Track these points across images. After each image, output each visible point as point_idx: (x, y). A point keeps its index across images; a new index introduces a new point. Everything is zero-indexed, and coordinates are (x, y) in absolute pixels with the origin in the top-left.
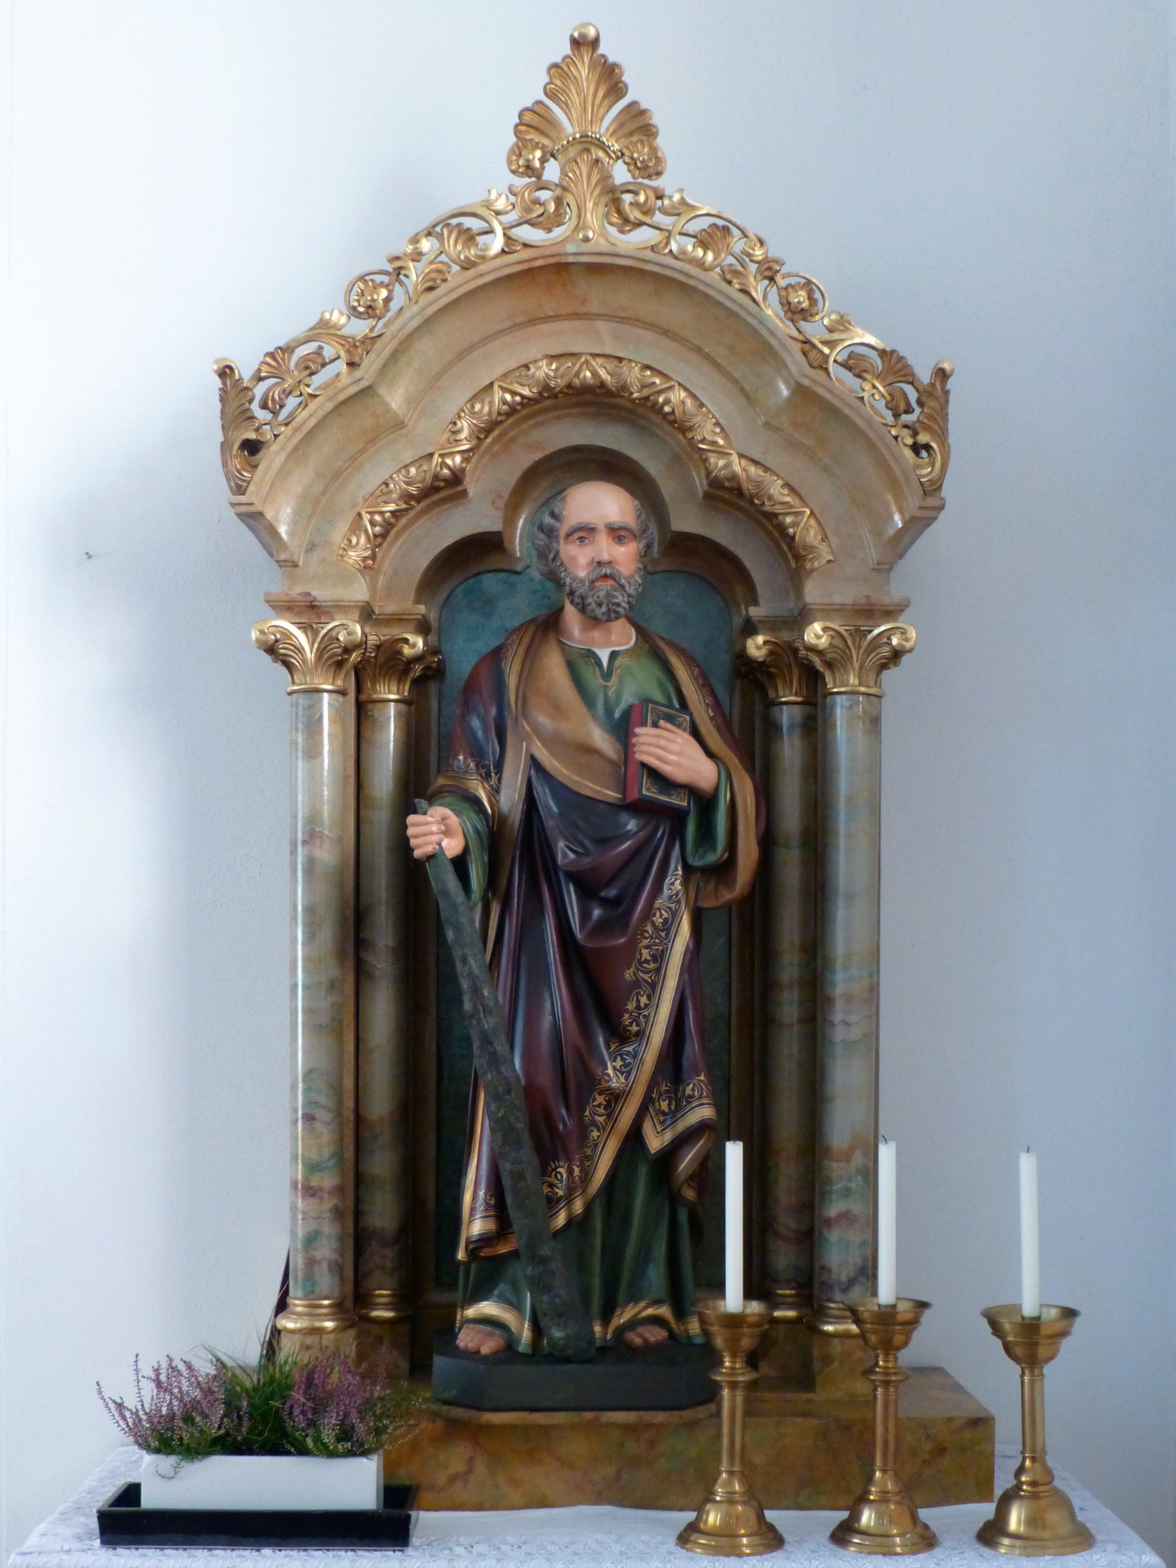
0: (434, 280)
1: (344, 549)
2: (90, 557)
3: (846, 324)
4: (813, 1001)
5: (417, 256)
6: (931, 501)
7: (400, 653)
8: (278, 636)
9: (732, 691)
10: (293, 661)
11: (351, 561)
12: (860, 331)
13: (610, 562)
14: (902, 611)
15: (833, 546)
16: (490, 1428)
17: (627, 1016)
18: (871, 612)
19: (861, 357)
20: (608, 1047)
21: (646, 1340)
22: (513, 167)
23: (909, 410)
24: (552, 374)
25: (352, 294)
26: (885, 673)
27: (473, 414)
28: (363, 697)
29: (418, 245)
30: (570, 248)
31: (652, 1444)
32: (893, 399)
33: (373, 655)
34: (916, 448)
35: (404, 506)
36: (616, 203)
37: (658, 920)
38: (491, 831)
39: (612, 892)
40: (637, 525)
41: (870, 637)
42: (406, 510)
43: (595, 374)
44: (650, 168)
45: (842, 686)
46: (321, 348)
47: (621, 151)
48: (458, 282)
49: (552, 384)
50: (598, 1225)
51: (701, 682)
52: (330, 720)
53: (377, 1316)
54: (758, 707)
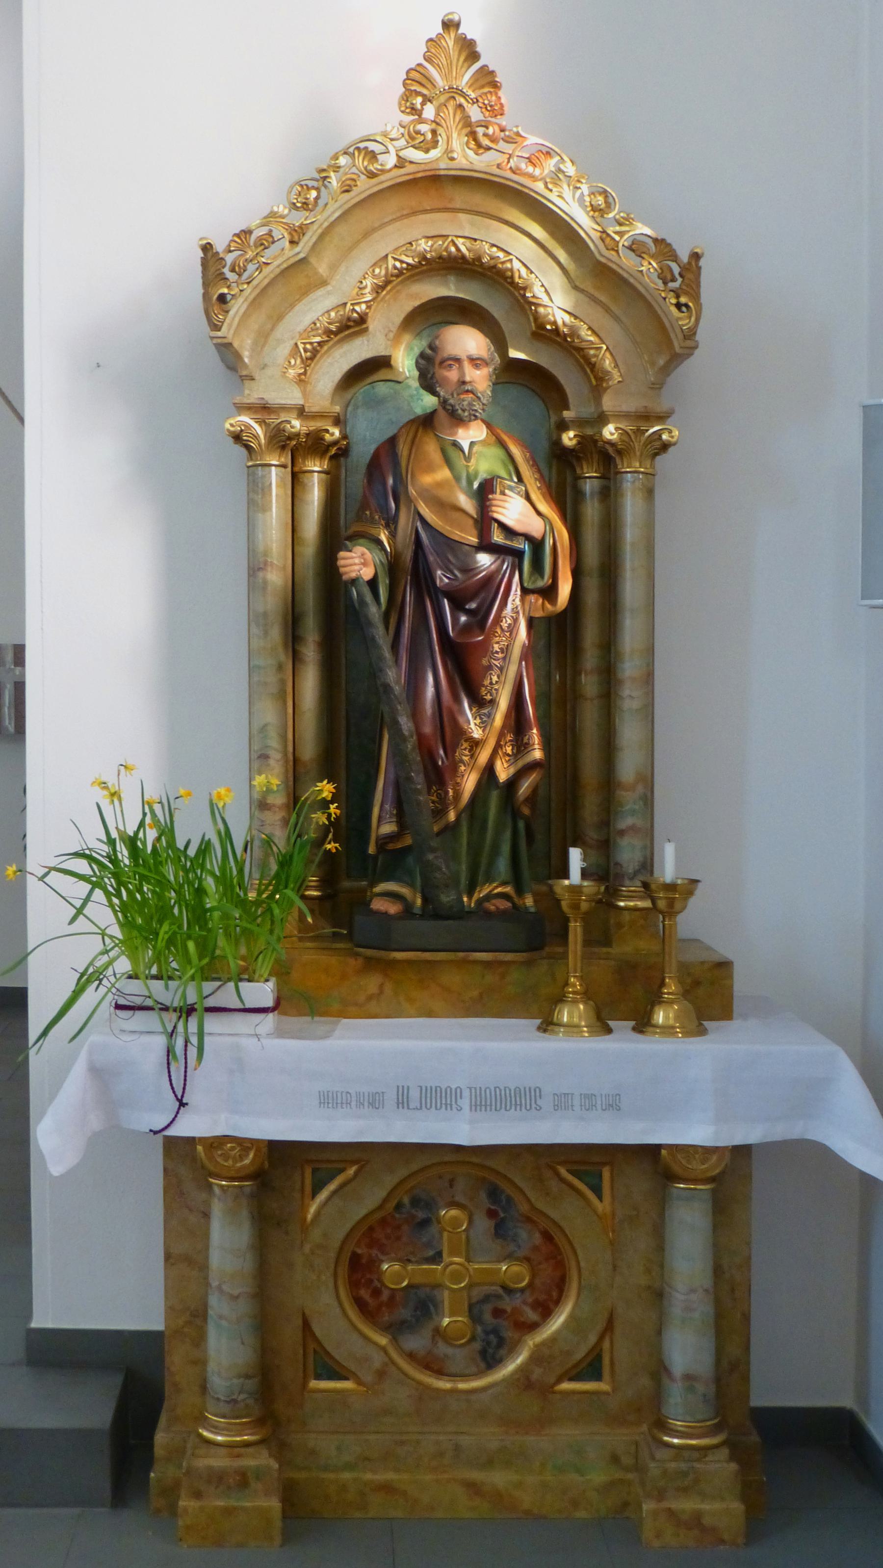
0: (350, 186)
1: (286, 368)
2: (99, 366)
3: (631, 221)
4: (609, 683)
5: (337, 168)
6: (689, 343)
7: (323, 439)
8: (243, 428)
9: (550, 467)
10: (252, 444)
11: (290, 376)
12: (639, 225)
13: (470, 382)
14: (669, 417)
15: (622, 371)
16: (396, 962)
17: (483, 689)
18: (647, 417)
19: (643, 244)
20: (471, 710)
21: (497, 908)
22: (403, 109)
23: (673, 280)
24: (428, 249)
25: (293, 193)
26: (658, 458)
27: (374, 276)
28: (296, 469)
29: (337, 162)
30: (442, 165)
31: (503, 976)
32: (663, 272)
33: (304, 440)
34: (678, 306)
35: (327, 339)
36: (473, 135)
37: (504, 625)
38: (389, 563)
39: (473, 605)
40: (488, 355)
41: (647, 434)
42: (327, 341)
43: (458, 249)
44: (496, 111)
45: (628, 467)
46: (271, 231)
47: (476, 99)
48: (364, 186)
49: (428, 256)
50: (464, 830)
51: (531, 463)
52: (277, 486)
53: (309, 895)
54: (569, 479)
